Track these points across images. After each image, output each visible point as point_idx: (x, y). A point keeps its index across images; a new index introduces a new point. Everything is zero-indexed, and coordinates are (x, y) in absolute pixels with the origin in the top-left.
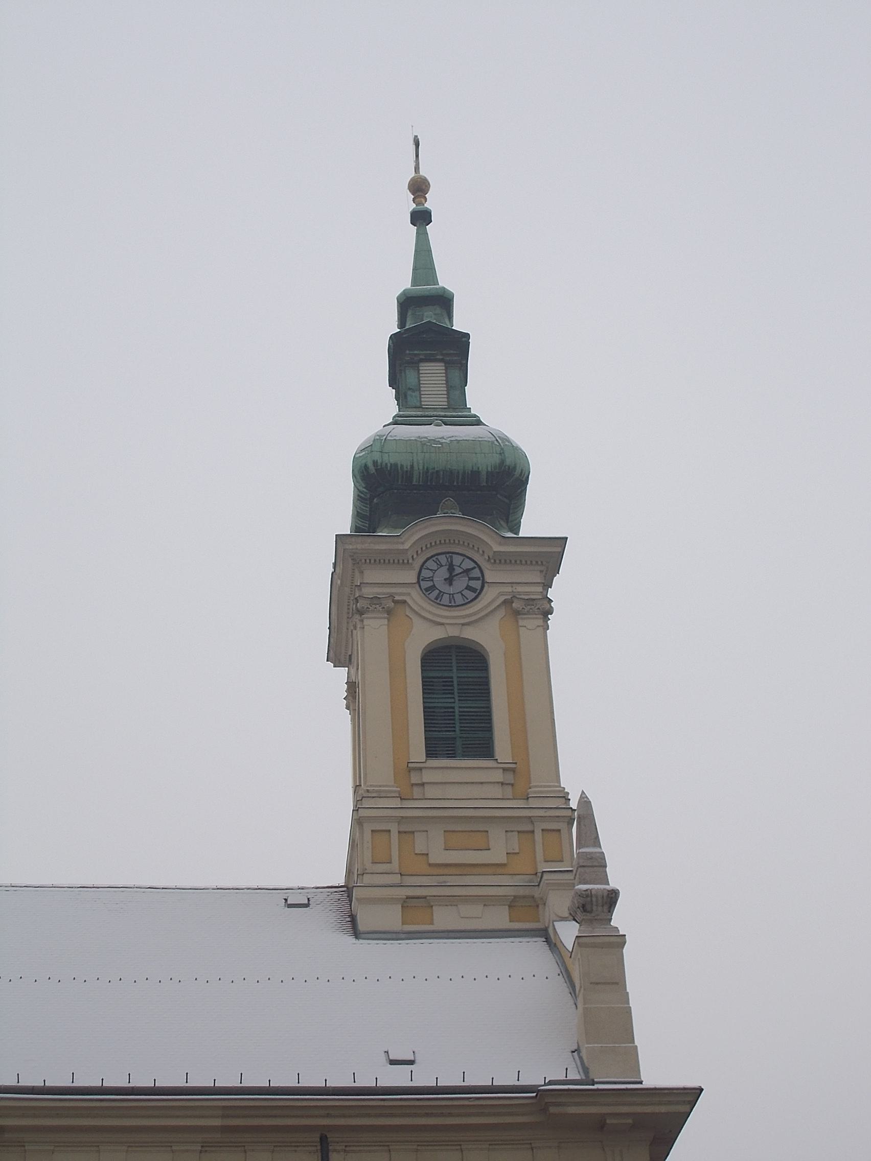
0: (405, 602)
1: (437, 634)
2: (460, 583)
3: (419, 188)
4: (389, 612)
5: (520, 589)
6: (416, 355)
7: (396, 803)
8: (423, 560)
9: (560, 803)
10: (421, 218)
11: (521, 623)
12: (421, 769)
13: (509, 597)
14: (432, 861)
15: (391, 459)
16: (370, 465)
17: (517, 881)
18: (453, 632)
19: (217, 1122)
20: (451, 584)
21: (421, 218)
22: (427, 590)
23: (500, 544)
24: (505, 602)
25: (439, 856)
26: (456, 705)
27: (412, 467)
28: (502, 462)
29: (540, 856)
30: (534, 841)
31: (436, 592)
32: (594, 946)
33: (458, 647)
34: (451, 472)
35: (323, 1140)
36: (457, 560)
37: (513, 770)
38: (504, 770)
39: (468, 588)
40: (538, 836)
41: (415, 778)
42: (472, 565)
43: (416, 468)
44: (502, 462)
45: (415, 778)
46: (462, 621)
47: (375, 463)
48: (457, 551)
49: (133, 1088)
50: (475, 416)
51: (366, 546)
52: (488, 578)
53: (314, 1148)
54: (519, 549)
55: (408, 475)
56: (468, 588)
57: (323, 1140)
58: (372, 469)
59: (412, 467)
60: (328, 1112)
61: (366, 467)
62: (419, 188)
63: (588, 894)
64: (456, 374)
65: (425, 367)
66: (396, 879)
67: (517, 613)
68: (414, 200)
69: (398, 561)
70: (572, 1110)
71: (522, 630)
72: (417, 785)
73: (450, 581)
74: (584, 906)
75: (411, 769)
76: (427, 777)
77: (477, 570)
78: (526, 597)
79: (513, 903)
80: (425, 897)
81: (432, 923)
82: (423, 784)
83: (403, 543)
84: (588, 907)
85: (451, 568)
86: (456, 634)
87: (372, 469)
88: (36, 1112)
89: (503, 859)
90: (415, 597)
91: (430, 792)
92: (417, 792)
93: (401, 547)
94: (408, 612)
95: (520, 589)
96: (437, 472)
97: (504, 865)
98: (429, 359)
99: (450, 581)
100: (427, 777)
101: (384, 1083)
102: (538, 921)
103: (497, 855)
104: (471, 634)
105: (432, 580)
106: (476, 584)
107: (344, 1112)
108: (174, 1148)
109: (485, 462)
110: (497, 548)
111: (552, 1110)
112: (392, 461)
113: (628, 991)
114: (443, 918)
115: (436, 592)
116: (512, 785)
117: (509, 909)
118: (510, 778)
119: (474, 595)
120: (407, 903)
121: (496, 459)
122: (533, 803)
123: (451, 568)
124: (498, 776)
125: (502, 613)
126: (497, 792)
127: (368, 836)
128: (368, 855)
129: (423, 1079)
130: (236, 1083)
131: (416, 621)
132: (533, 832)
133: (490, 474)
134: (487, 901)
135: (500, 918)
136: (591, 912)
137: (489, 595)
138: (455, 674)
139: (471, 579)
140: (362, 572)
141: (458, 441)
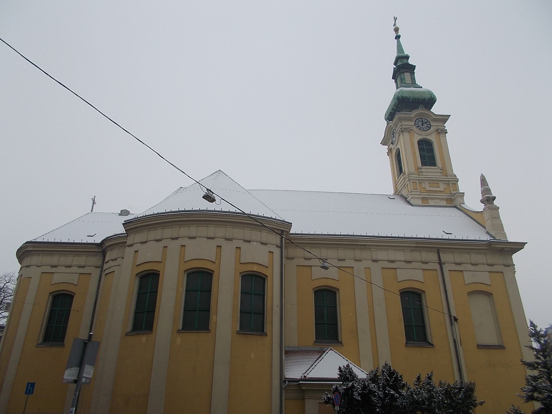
0: (412, 129)
1: (421, 137)
2: (425, 125)
3: (396, 30)
4: (409, 131)
5: (439, 127)
6: (403, 71)
7: (417, 176)
8: (415, 120)
9: (455, 177)
10: (398, 37)
11: (440, 135)
12: (421, 168)
13: (437, 129)
14: (426, 189)
15: (405, 95)
16: (400, 96)
17: (446, 195)
18: (424, 137)
19: (415, 245)
20: (423, 125)
21: (398, 37)
22: (417, 127)
23: (435, 116)
24: (436, 130)
25: (428, 188)
26: (426, 154)
27: (410, 97)
28: (431, 97)
29: (452, 189)
30: (450, 186)
31: (419, 127)
32: (492, 209)
33: (425, 141)
34: (419, 99)
35: (438, 250)
36: (423, 120)
37: (442, 169)
38: (441, 169)
39: (427, 126)
40: (451, 185)
41: (420, 170)
42: (427, 121)
43: (411, 98)
44: (431, 97)
45: (420, 170)
46: (427, 134)
47: (401, 96)
48: (423, 118)
49: (96, 243)
50: (420, 86)
51: (403, 116)
52: (431, 124)
53: (435, 252)
54: (441, 118)
55: (409, 99)
56: (427, 126)
57: (438, 250)
58: (400, 98)
59: (410, 97)
60: (440, 244)
61: (399, 97)
62: (396, 30)
63: (489, 197)
64: (412, 75)
65: (405, 74)
66: (419, 193)
67: (439, 133)
68: (396, 33)
69: (410, 120)
70: (497, 246)
71: (441, 137)
72: (420, 172)
73: (422, 125)
74: (488, 200)
75: (418, 168)
76: (423, 170)
77: (429, 122)
78: (441, 129)
79: (447, 200)
80: (427, 198)
81: (428, 204)
82: (422, 172)
83: (412, 115)
84: (488, 200)
85: (422, 122)
86: (425, 137)
87: (400, 98)
88: (374, 241)
89: (443, 190)
90: (415, 128)
91: (424, 174)
92: (421, 174)
93: (411, 116)
94: (413, 132)
95: (439, 127)
96: (416, 99)
97: (443, 191)
98: (406, 72)
99: (422, 125)
100: (423, 170)
101: (444, 238)
102: (453, 204)
103: (442, 189)
104: (428, 137)
105: (418, 124)
106: (429, 126)
107: (443, 244)
108: (404, 251)
109: (427, 97)
110: (434, 117)
111: (493, 246)
112: (405, 96)
113: (501, 219)
114: (431, 202)
115: (419, 127)
116: (442, 173)
117: (446, 202)
118: (442, 171)
119: (422, 130)
120: (423, 199)
121: (430, 96)
122: (448, 177)
123: (422, 122)
124: (440, 171)
125: (435, 133)
126: (440, 174)
127: (411, 183)
128: (412, 187)
129: (451, 237)
130: (403, 236)
131: (415, 134)
132: (449, 184)
133: (428, 99)
134: (441, 199)
135: (444, 203)
136: (489, 201)
137: (432, 128)
138: (425, 147)
139: (427, 124)
140: (401, 122)
141: (420, 92)
